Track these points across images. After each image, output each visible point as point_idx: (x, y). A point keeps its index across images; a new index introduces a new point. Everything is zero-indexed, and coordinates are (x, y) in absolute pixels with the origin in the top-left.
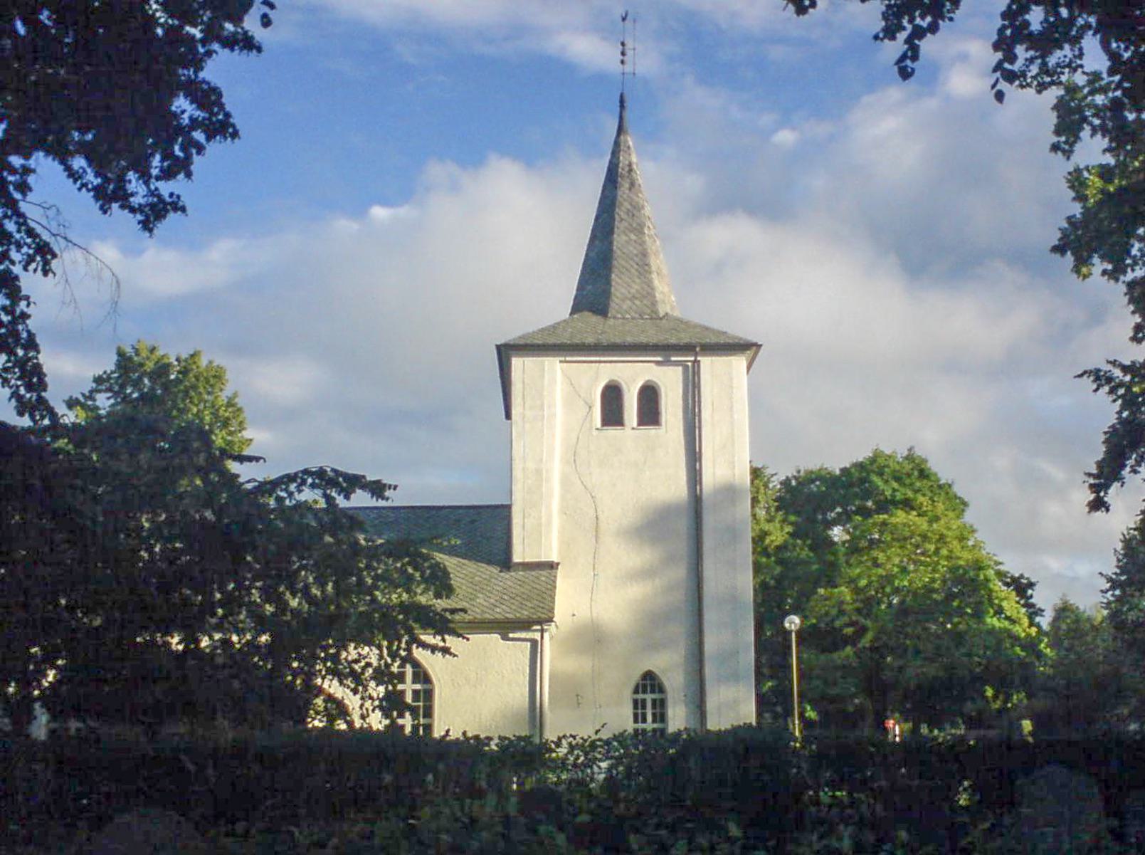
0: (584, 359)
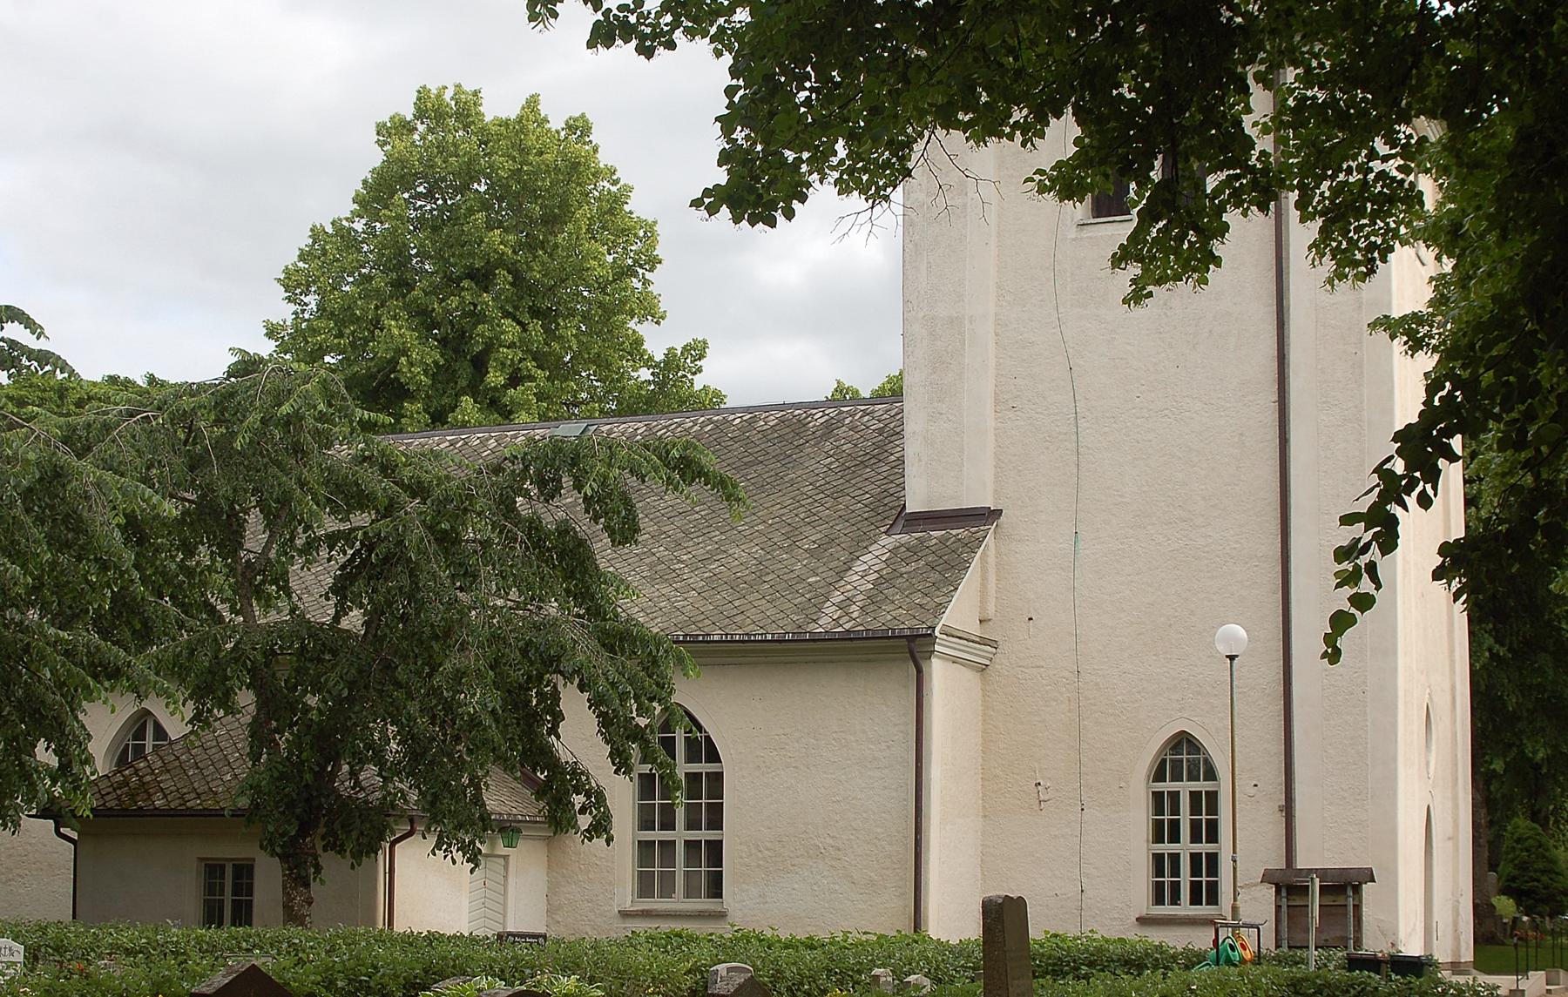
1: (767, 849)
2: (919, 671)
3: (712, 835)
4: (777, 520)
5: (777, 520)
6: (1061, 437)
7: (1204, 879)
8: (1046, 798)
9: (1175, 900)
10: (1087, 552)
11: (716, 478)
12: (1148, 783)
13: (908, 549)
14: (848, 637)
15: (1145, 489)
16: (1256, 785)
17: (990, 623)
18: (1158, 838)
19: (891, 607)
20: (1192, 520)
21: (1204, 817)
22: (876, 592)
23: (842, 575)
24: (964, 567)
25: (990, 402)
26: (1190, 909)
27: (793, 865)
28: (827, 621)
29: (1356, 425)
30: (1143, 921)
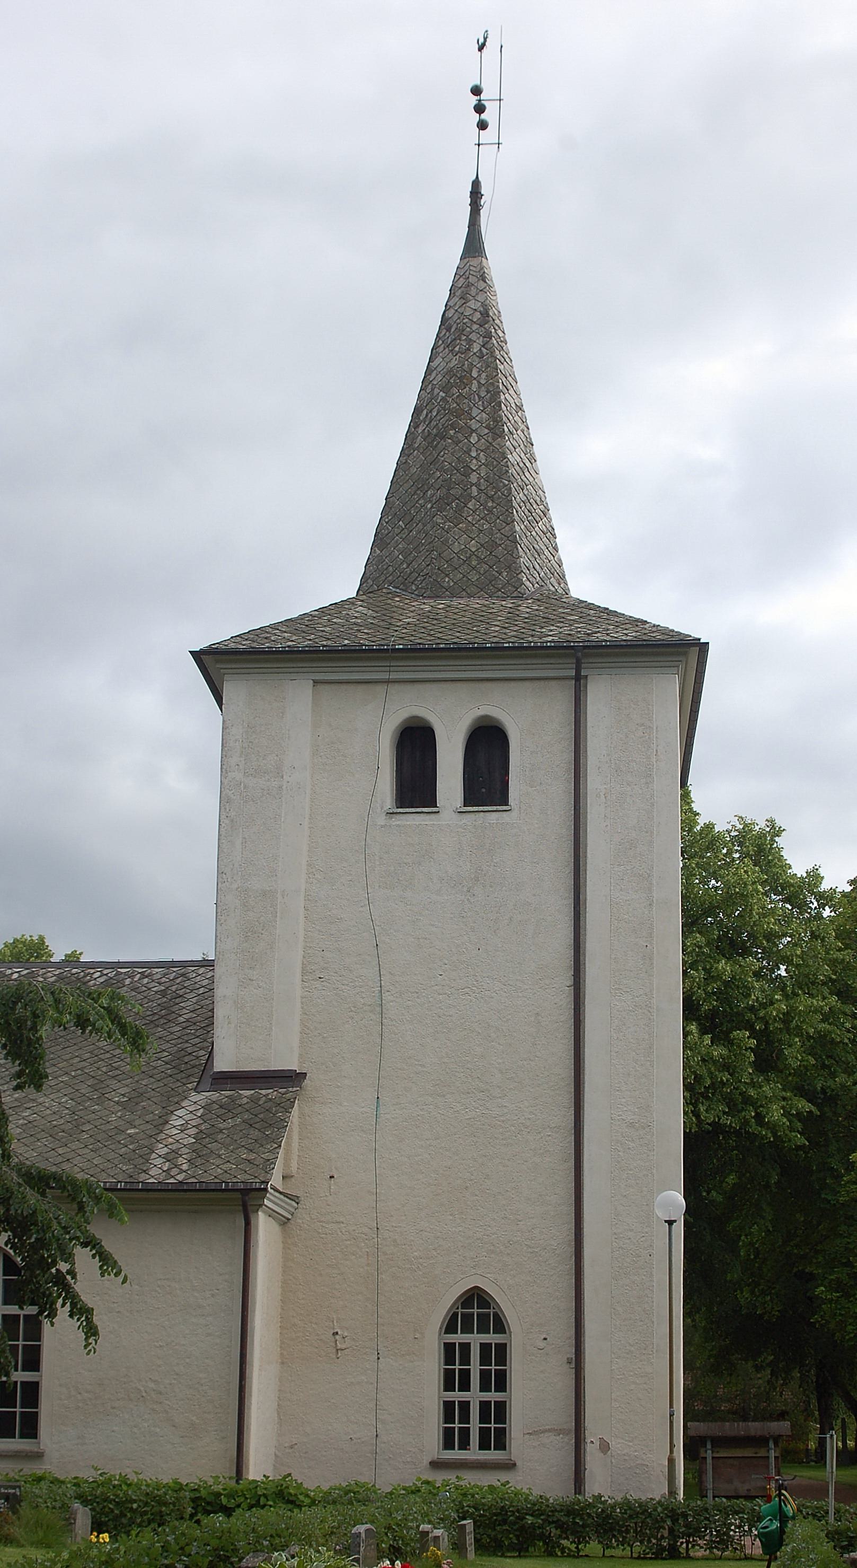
0: (241, 666)
1: (87, 1392)
2: (248, 1223)
3: (28, 1376)
4: (79, 1072)
5: (79, 1072)
6: (366, 1008)
7: (457, 1425)
8: (343, 1347)
9: (464, 1445)
10: (388, 1116)
11: (132, 1028)
12: (440, 1334)
13: (221, 1107)
14: (181, 1188)
15: (446, 1060)
16: (545, 1339)
17: (293, 1180)
18: (449, 1386)
19: (218, 1162)
20: (489, 1091)
21: (457, 1367)
22: (200, 1146)
23: (160, 1128)
24: (282, 1125)
25: (298, 971)
26: (479, 1454)
27: (114, 1408)
28: (156, 1172)
29: (646, 1012)
30: (436, 1465)
